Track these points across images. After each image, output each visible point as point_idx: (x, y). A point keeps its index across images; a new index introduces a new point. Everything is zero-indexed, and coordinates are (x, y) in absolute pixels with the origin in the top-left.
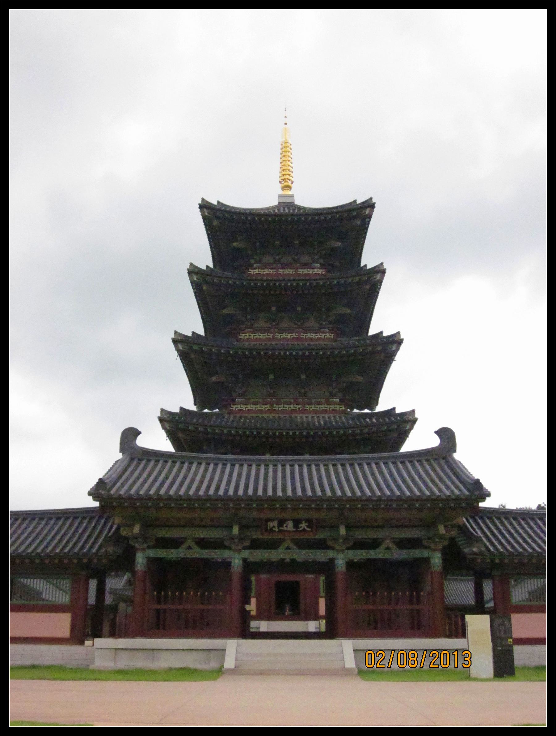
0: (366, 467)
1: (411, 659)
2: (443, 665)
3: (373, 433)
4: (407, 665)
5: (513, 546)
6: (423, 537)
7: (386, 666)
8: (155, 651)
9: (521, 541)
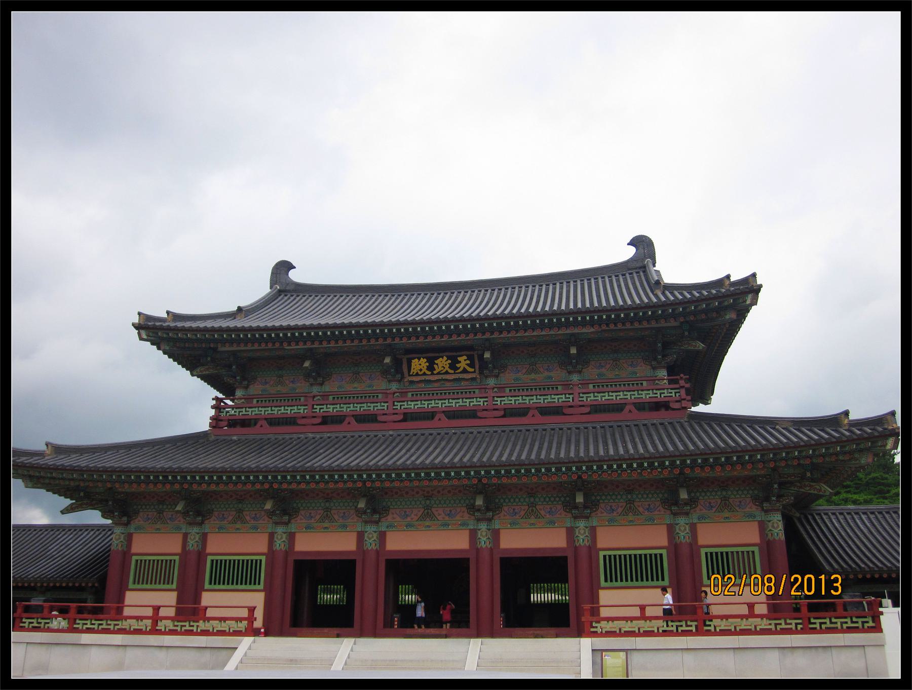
0: (614, 279)
1: (767, 584)
2: (713, 592)
3: (794, 458)
4: (763, 592)
5: (866, 564)
6: (667, 393)
7: (737, 594)
8: (128, 648)
9: (81, 556)
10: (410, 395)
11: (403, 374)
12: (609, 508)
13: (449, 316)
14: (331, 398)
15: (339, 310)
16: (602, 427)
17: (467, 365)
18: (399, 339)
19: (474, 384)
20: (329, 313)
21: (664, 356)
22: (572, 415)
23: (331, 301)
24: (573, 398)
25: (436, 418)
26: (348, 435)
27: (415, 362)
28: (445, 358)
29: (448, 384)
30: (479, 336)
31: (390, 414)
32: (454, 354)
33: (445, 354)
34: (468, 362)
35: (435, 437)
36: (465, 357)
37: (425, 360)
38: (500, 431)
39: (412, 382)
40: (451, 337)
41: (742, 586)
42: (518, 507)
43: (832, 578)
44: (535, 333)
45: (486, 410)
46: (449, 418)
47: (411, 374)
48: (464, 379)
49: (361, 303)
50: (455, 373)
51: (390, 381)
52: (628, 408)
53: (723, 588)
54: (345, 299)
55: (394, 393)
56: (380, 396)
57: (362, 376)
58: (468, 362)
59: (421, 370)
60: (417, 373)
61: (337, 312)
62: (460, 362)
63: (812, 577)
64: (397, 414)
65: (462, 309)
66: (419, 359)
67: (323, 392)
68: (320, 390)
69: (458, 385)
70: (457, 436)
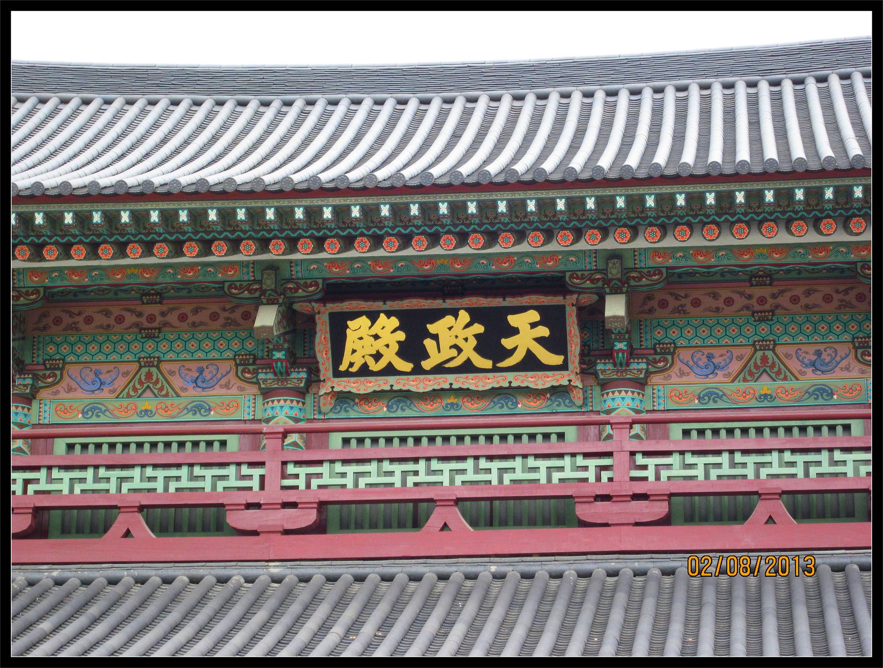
1: (743, 566)
10: (336, 440)
11: (314, 371)
12: (704, 359)
13: (265, 178)
14: (60, 446)
15: (88, 146)
16: (838, 569)
17: (540, 340)
18: (396, 243)
19: (562, 409)
20: (53, 154)
22: (606, 525)
23: (51, 116)
24: (262, 477)
25: (434, 522)
26: (127, 574)
27: (358, 327)
28: (464, 317)
29: (469, 408)
30: (247, 254)
31: (271, 506)
33: (467, 301)
34: (544, 331)
35: (210, 589)
37: (394, 322)
38: (657, 572)
39: (343, 398)
40: (179, 253)
42: (724, 351)
44: (669, 242)
45: (606, 498)
46: (474, 523)
47: (343, 368)
48: (527, 391)
49: (156, 125)
50: (495, 369)
51: (267, 394)
52: (761, 510)
54: (100, 111)
55: (285, 434)
56: (233, 442)
57: (171, 373)
58: (544, 331)
59: (377, 356)
60: (365, 366)
61: (81, 151)
62: (515, 331)
64: (294, 505)
65: (291, 158)
66: (373, 317)
67: (34, 426)
68: (300, 415)
69: (505, 411)
70: (424, 586)
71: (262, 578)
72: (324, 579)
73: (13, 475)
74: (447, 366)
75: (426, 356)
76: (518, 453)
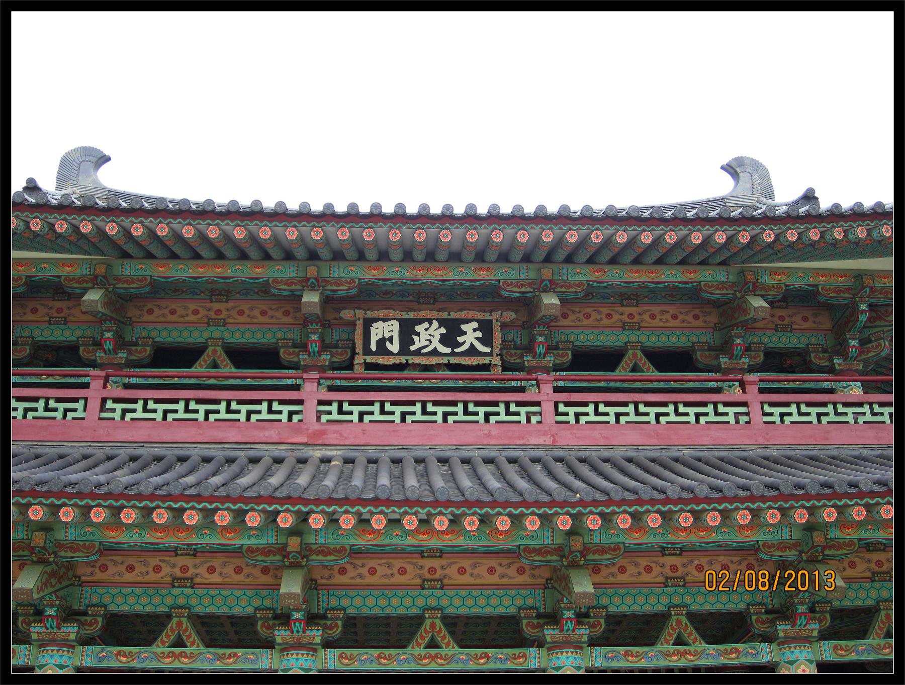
17: (477, 339)
21: (863, 342)
28: (435, 324)
32: (453, 316)
34: (479, 334)
36: (475, 325)
41: (737, 581)
43: (786, 576)
53: (718, 584)
58: (479, 334)
62: (465, 333)
63: (806, 573)
71: (266, 458)
72: (271, 461)
73: (14, 404)
74: (423, 351)
75: (413, 343)
76: (151, 397)
